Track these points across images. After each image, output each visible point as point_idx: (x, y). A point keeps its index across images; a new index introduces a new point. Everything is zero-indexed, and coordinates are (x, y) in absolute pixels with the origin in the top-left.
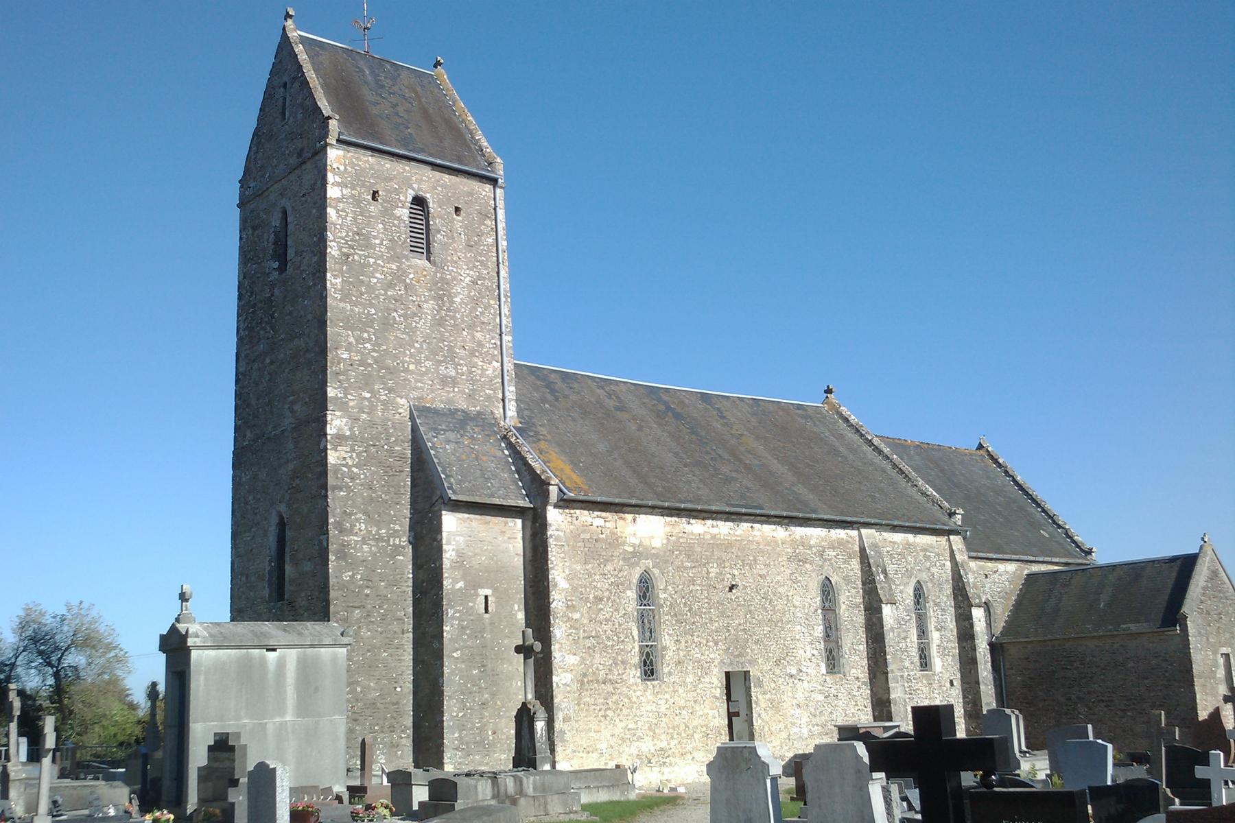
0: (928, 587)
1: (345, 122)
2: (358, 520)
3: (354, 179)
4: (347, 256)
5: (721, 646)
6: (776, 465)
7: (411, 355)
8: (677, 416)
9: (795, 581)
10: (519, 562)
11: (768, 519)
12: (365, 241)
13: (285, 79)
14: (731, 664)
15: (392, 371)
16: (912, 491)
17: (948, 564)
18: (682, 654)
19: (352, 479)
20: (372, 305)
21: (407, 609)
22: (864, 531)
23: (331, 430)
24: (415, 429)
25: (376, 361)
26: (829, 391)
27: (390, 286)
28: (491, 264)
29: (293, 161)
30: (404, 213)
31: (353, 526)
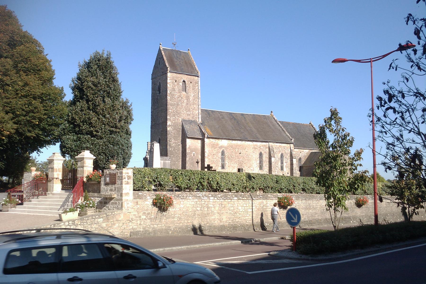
0: (284, 154)
1: (171, 67)
2: (172, 140)
3: (173, 79)
4: (171, 93)
5: (237, 164)
6: (254, 129)
7: (182, 110)
8: (235, 119)
9: (254, 152)
10: (200, 148)
11: (248, 141)
12: (174, 90)
13: (160, 57)
14: (239, 167)
15: (179, 113)
16: (285, 135)
17: (289, 150)
18: (229, 165)
19: (172, 133)
20: (175, 101)
21: (181, 155)
22: (270, 143)
23: (168, 124)
24: (182, 124)
25: (176, 111)
26: (272, 112)
27: (179, 98)
28: (197, 92)
29: (161, 74)
30: (181, 84)
31: (172, 141)
